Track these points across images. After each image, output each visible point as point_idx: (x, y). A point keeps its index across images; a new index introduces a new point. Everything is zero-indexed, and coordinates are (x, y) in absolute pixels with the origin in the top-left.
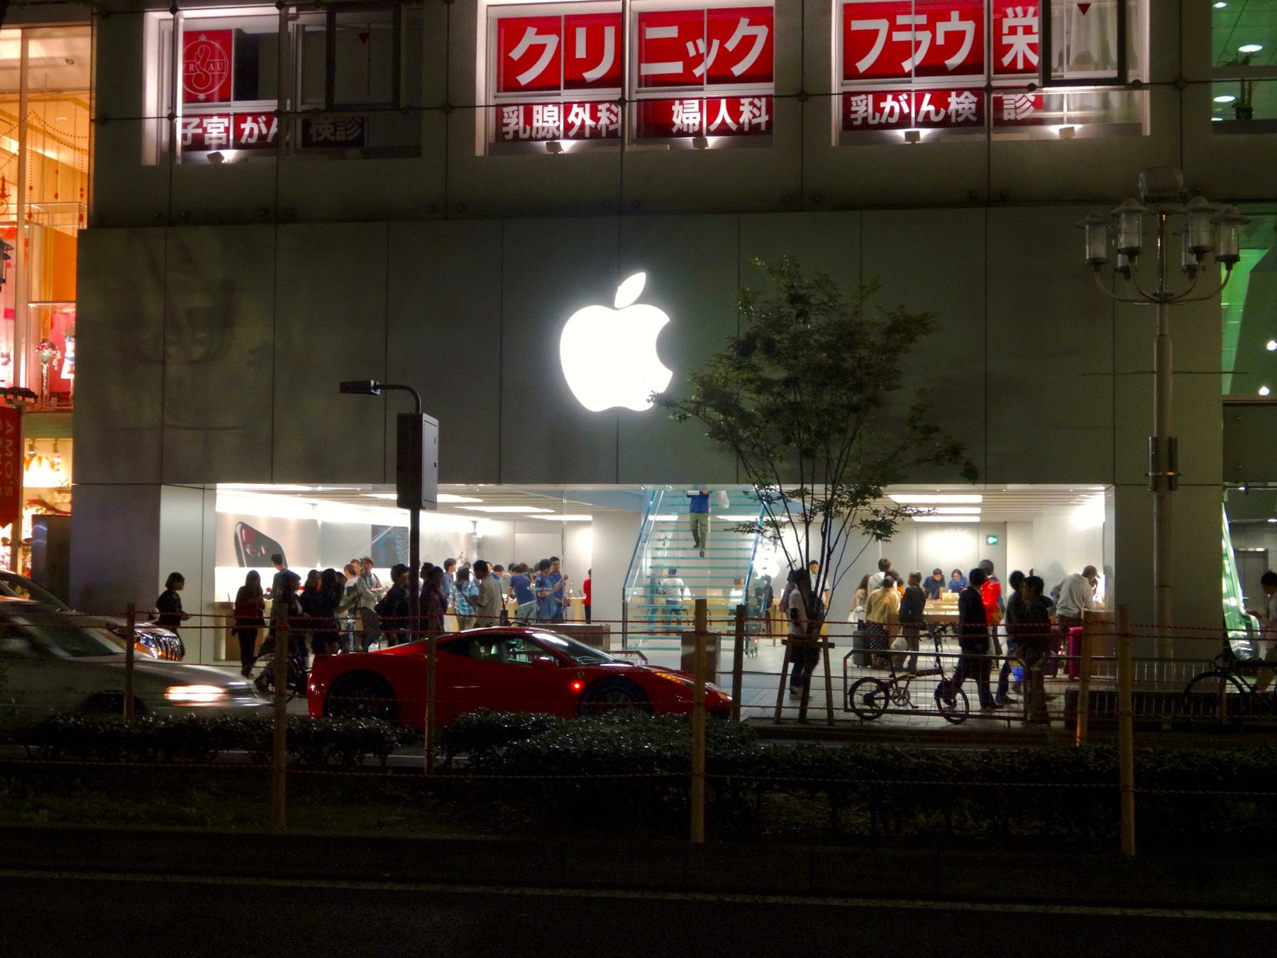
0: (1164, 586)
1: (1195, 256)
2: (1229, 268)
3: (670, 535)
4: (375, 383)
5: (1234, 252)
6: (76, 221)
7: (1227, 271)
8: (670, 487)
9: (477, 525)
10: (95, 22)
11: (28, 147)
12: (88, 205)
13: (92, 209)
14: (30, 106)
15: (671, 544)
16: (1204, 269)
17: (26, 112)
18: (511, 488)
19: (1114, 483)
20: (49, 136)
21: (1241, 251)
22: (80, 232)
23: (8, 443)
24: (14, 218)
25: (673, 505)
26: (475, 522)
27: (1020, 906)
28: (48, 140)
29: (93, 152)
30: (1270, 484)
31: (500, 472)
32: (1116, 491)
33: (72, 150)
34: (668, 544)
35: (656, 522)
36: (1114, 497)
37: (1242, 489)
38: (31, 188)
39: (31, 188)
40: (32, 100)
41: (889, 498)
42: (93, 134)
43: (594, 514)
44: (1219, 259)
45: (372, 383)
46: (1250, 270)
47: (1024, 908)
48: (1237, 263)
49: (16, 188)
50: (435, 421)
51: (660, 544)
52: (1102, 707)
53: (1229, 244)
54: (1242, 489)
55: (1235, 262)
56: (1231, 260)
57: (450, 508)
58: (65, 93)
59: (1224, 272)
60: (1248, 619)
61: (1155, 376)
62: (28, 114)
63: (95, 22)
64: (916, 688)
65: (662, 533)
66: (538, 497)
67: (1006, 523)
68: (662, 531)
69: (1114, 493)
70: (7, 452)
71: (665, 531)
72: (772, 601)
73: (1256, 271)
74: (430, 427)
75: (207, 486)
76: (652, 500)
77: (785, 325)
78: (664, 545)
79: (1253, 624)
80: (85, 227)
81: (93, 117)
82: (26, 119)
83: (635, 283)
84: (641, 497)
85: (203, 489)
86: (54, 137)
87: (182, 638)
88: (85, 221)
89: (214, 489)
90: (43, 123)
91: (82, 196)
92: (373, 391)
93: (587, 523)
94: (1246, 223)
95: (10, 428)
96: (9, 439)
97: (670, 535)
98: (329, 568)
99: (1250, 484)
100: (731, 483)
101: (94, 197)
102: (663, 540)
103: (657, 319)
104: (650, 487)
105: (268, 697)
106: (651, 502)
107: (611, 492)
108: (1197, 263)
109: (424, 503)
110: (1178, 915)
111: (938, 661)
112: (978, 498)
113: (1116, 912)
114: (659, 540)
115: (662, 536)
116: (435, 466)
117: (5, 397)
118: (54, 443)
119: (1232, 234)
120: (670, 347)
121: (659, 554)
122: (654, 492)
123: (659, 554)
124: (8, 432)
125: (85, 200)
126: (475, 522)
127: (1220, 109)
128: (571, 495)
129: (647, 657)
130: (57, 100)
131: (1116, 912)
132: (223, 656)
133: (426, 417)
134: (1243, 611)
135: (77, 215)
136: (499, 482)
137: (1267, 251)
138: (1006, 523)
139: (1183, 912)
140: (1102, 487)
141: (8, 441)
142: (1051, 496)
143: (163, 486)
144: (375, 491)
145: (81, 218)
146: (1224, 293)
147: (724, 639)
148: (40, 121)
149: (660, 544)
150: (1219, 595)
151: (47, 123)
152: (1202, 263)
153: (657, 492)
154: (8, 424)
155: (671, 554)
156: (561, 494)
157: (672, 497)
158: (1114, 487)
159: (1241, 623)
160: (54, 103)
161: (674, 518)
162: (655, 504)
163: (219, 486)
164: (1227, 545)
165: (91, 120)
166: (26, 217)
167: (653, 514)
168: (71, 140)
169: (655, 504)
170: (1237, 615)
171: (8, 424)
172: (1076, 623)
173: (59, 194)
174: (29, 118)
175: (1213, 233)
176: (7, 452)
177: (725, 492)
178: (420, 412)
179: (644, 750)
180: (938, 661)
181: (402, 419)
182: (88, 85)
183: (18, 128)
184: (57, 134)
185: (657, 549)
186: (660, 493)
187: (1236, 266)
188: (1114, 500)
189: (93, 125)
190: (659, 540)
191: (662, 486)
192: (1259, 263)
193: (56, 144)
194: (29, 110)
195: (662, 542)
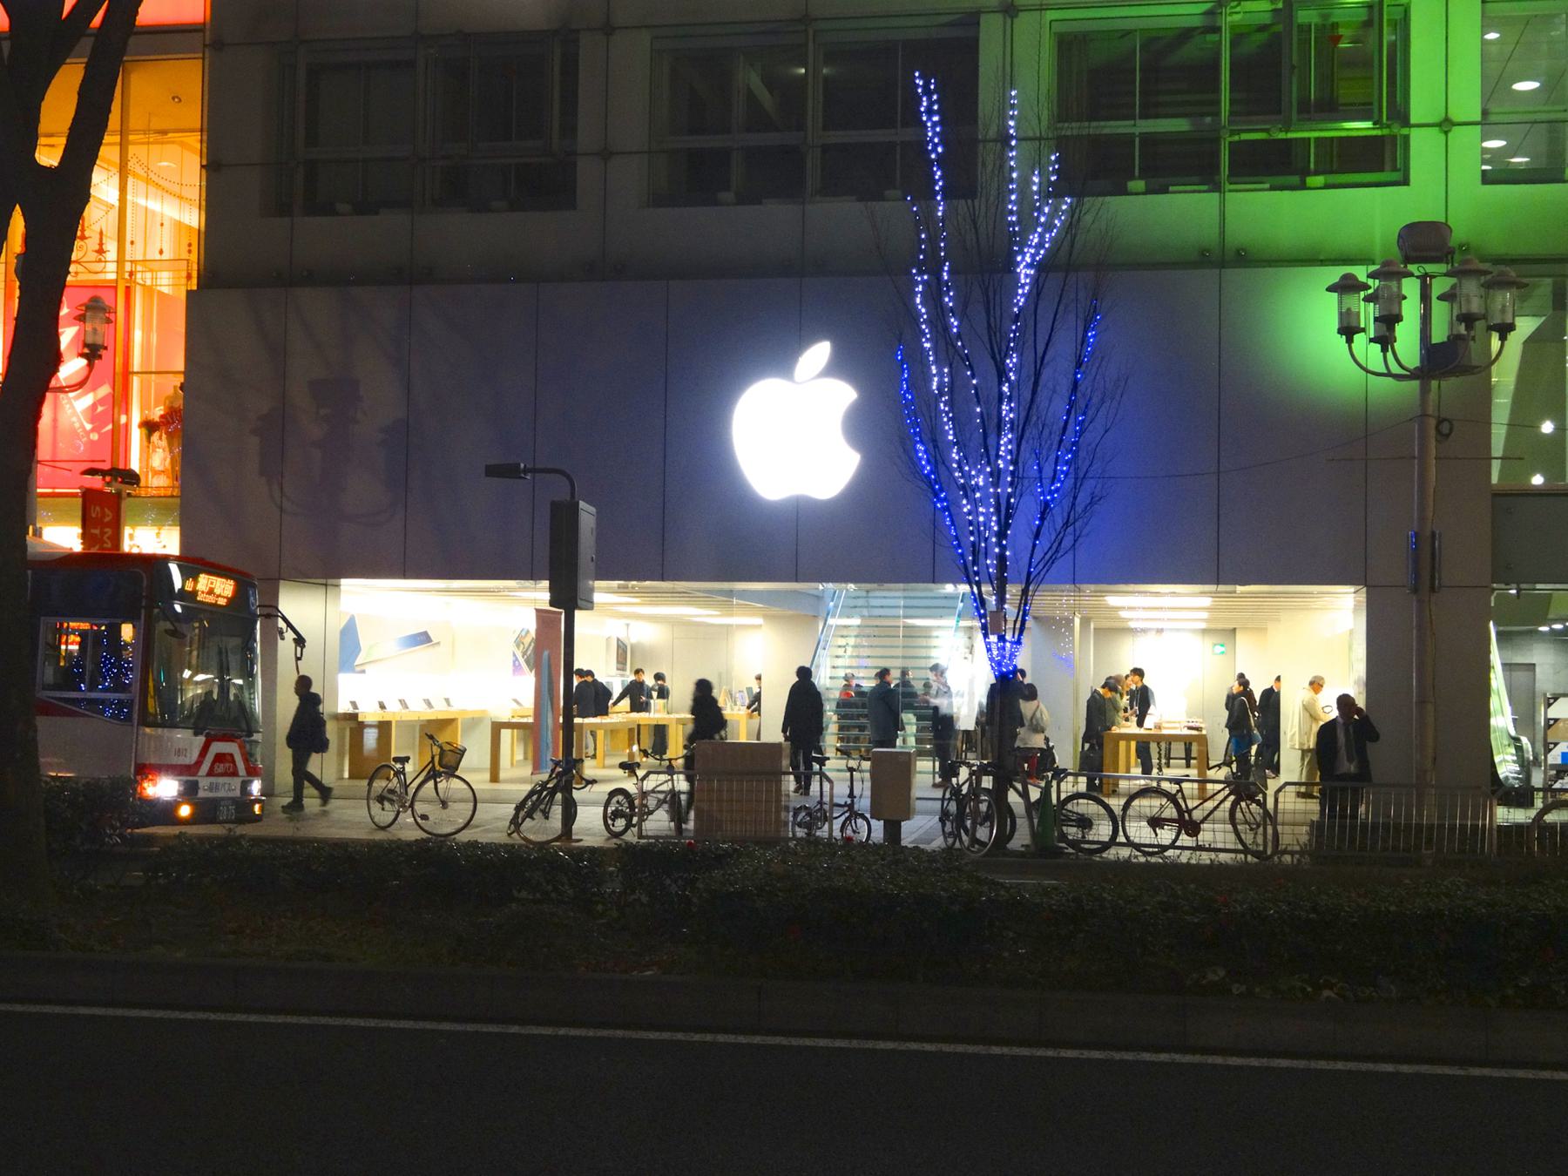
0: (1424, 702)
1: (1463, 325)
2: (1503, 338)
3: (852, 641)
4: (525, 466)
5: (1509, 320)
6: (184, 281)
7: (1500, 342)
8: (851, 586)
9: (630, 627)
10: (207, 55)
11: (129, 197)
12: (198, 263)
13: (202, 268)
14: (132, 149)
15: (852, 652)
16: (1473, 339)
17: (127, 157)
19: (1366, 586)
20: (155, 184)
21: (1517, 319)
22: (189, 293)
23: (106, 533)
24: (112, 276)
25: (855, 607)
26: (628, 625)
27: (1279, 1061)
28: (152, 189)
29: (204, 203)
30: (1539, 586)
32: (1368, 593)
33: (178, 201)
35: (838, 627)
36: (1365, 600)
37: (1514, 592)
38: (132, 243)
39: (132, 243)
40: (135, 143)
41: (1105, 600)
42: (204, 183)
43: (765, 617)
44: (1491, 328)
45: (522, 465)
46: (1522, 342)
47: (1284, 1063)
48: (1512, 333)
49: (116, 244)
50: (592, 509)
51: (840, 652)
52: (1352, 841)
53: (1503, 310)
54: (1514, 592)
55: (1510, 332)
56: (1505, 330)
58: (170, 135)
59: (1495, 343)
60: (1517, 740)
61: (1416, 461)
62: (129, 158)
63: (207, 55)
65: (843, 639)
67: (1235, 629)
68: (842, 636)
69: (1365, 595)
70: (107, 543)
71: (847, 637)
72: (780, 790)
73: (1531, 342)
74: (587, 514)
75: (330, 581)
76: (832, 601)
78: (845, 652)
79: (1524, 746)
80: (195, 288)
81: (204, 163)
82: (127, 164)
83: (819, 353)
84: (819, 598)
85: (326, 585)
86: (157, 185)
87: (975, 369)
88: (195, 281)
89: (338, 586)
90: (146, 169)
91: (190, 251)
94: (1520, 286)
95: (108, 516)
96: (108, 527)
98: (331, 746)
99: (1523, 586)
100: (928, 582)
101: (205, 258)
102: (844, 647)
103: (844, 394)
104: (830, 585)
106: (832, 604)
108: (1465, 333)
110: (1462, 1072)
112: (1207, 601)
113: (1389, 1068)
114: (840, 647)
115: (842, 642)
117: (104, 479)
118: (157, 531)
119: (1505, 297)
120: (860, 426)
121: (839, 662)
122: (835, 592)
123: (839, 662)
124: (107, 519)
125: (194, 257)
126: (628, 625)
127: (1489, 156)
128: (743, 595)
130: (162, 143)
131: (1389, 1068)
132: (346, 775)
133: (582, 504)
134: (1513, 733)
135: (184, 274)
137: (1544, 318)
138: (1235, 629)
139: (1466, 1069)
140: (1351, 589)
141: (107, 530)
142: (1279, 599)
143: (282, 582)
145: (189, 277)
146: (1494, 368)
147: (920, 760)
148: (143, 166)
149: (840, 652)
150: (1486, 714)
151: (152, 168)
152: (1472, 333)
154: (106, 510)
157: (854, 598)
158: (1365, 589)
159: (1509, 745)
160: (158, 147)
162: (836, 607)
163: (344, 582)
164: (1495, 658)
165: (202, 166)
166: (127, 276)
167: (833, 616)
168: (176, 189)
169: (836, 607)
170: (1505, 736)
171: (106, 510)
173: (164, 250)
174: (129, 164)
175: (1486, 298)
176: (107, 543)
177: (603, 731)
178: (576, 499)
179: (1353, 720)
181: (555, 507)
182: (199, 126)
183: (118, 174)
184: (161, 182)
185: (837, 657)
186: (841, 592)
187: (1512, 336)
188: (1365, 604)
189: (204, 171)
190: (840, 647)
191: (843, 585)
192: (1533, 333)
193: (159, 192)
194: (130, 155)
195: (844, 649)
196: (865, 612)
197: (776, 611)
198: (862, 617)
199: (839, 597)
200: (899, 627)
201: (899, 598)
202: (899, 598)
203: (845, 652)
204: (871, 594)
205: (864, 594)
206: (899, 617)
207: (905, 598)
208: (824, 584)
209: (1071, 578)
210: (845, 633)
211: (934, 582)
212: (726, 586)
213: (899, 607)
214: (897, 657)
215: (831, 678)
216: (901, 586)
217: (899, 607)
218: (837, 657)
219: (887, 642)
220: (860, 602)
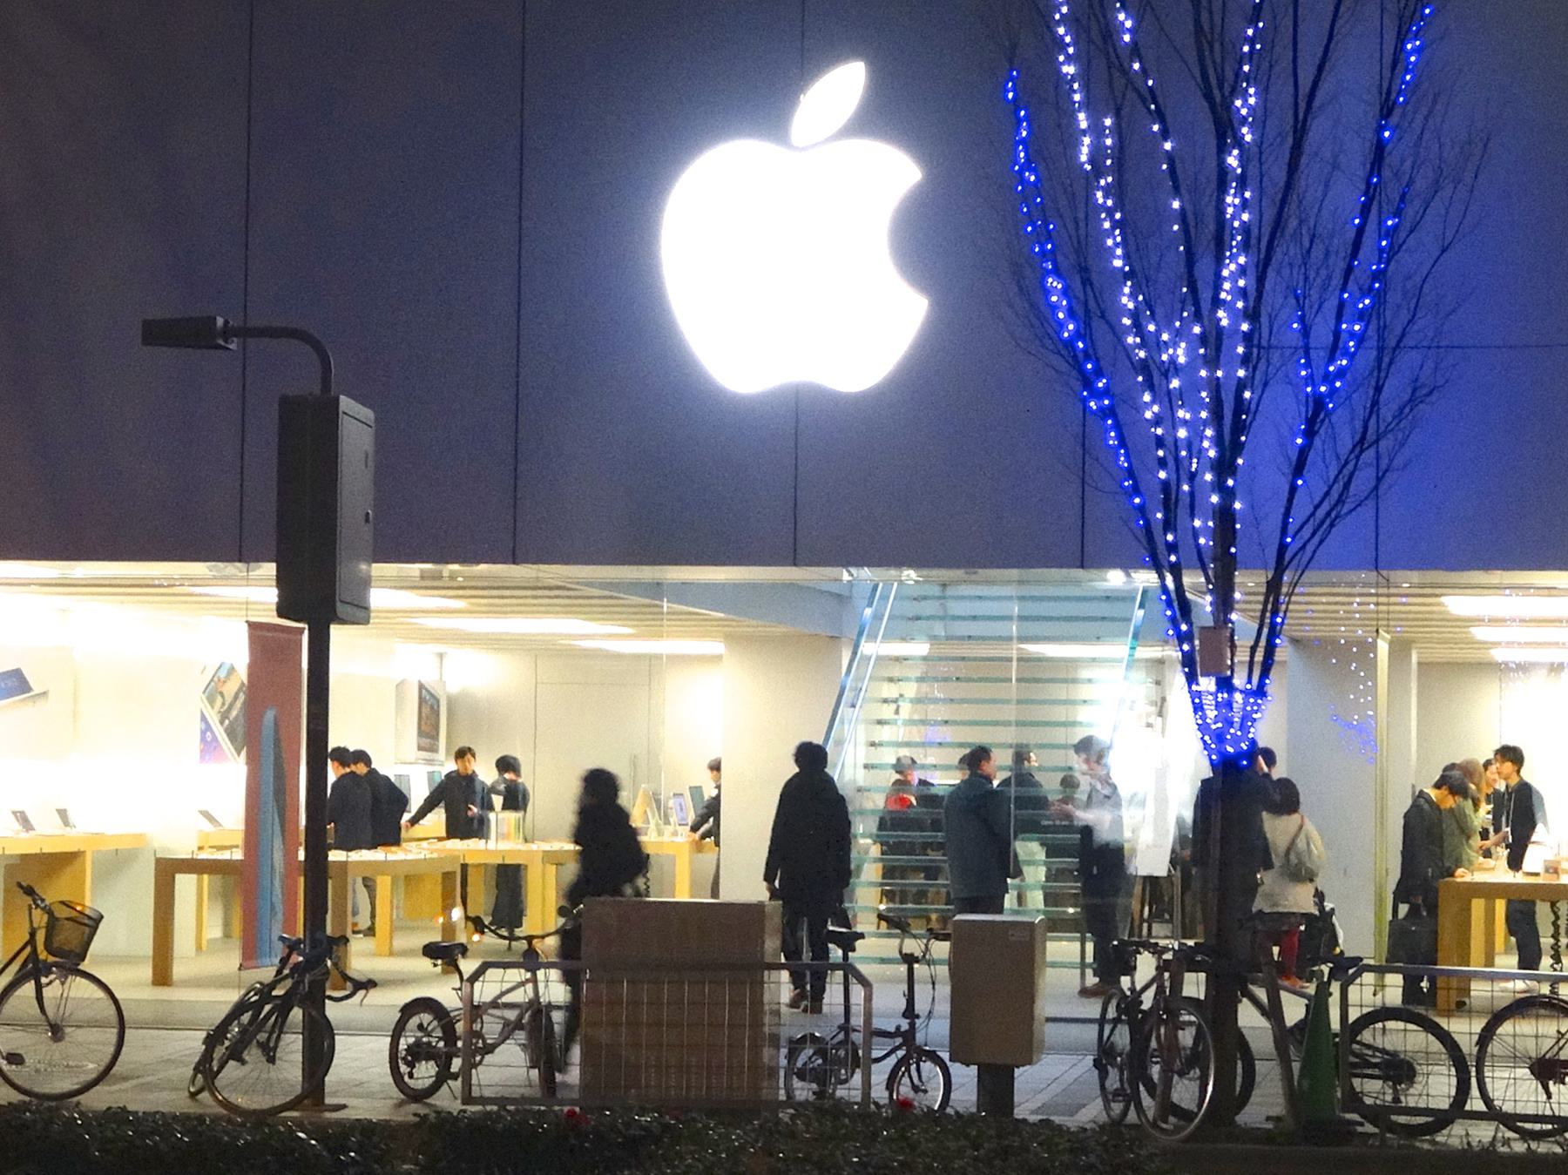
3: (910, 689)
4: (226, 322)
8: (910, 575)
18: (814, 576)
25: (918, 618)
26: (441, 656)
31: (1377, 558)
34: (906, 709)
35: (880, 658)
43: (730, 638)
50: (367, 414)
51: (887, 712)
57: (407, 627)
64: (1427, 1053)
66: (649, 606)
68: (891, 680)
76: (870, 605)
77: (1466, 165)
78: (897, 712)
84: (842, 599)
92: (221, 342)
93: (717, 658)
97: (910, 689)
102: (895, 701)
104: (866, 573)
105: (1100, 1126)
106: (868, 612)
107: (774, 586)
109: (341, 609)
111: (530, 944)
114: (885, 701)
115: (889, 691)
116: (367, 520)
121: (885, 733)
122: (875, 588)
123: (885, 733)
126: (441, 656)
128: (683, 592)
129: (870, 979)
133: (345, 403)
136: (514, 560)
144: (225, 580)
149: (887, 712)
153: (881, 585)
155: (916, 735)
156: (656, 590)
161: (920, 648)
162: (878, 617)
167: (873, 637)
169: (878, 617)
172: (392, 841)
180: (530, 944)
181: (290, 408)
185: (880, 722)
186: (888, 586)
190: (885, 701)
191: (893, 572)
195: (893, 707)
196: (939, 629)
197: (749, 626)
198: (933, 638)
199: (885, 598)
200: (1010, 660)
201: (1010, 598)
202: (1010, 598)
203: (897, 712)
204: (950, 592)
205: (936, 590)
206: (1010, 639)
207: (1022, 598)
208: (853, 570)
209: (1371, 555)
210: (896, 673)
211: (1082, 567)
212: (647, 573)
213: (1010, 618)
214: (1007, 724)
215: (866, 766)
216: (1014, 573)
217: (1010, 618)
218: (880, 722)
219: (986, 691)
220: (929, 608)
